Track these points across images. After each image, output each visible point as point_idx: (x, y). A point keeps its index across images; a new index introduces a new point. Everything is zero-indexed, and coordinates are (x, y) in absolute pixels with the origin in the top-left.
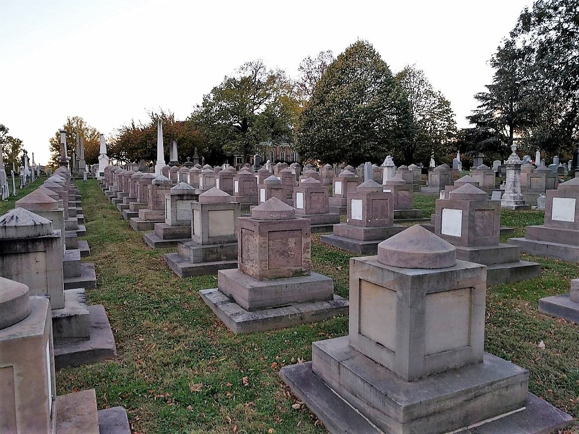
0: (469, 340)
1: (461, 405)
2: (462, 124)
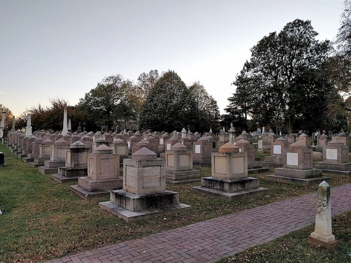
0: (189, 165)
1: (186, 175)
2: (222, 112)
